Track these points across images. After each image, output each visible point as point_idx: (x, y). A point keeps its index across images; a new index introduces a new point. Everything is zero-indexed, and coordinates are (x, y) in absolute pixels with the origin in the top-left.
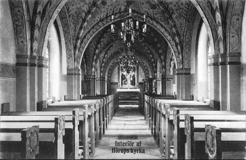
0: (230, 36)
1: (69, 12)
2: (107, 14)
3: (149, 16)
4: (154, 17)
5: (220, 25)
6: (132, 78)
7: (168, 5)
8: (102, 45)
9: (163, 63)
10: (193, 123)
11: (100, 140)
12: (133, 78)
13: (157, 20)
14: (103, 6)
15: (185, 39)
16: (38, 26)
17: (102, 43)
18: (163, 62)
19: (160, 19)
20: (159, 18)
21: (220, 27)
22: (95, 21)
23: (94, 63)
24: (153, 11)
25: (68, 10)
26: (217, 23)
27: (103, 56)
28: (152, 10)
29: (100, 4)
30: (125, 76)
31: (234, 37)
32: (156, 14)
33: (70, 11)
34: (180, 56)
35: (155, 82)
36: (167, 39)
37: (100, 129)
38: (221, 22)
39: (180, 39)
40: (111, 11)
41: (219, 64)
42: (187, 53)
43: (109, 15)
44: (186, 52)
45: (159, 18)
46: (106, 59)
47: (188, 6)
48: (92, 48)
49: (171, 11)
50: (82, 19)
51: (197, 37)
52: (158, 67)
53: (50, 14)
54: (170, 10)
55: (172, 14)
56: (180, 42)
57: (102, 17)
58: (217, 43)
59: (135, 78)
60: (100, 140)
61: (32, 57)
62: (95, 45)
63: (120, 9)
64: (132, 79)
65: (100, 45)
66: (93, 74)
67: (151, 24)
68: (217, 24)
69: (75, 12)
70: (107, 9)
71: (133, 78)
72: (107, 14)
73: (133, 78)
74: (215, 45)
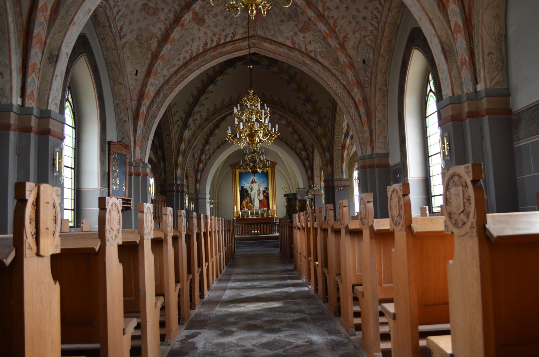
0: (483, 53)
1: (123, 37)
2: (206, 44)
3: (297, 47)
4: (306, 49)
5: (459, 31)
6: (261, 195)
7: (335, 23)
8: (197, 120)
9: (327, 154)
10: (417, 232)
11: (191, 309)
12: (265, 194)
13: (312, 55)
14: (196, 27)
15: (373, 92)
16: (41, 39)
17: (197, 116)
18: (327, 152)
19: (320, 52)
20: (318, 50)
21: (459, 35)
22: (179, 60)
23: (180, 158)
24: (304, 37)
25: (120, 33)
26: (453, 26)
27: (178, 29)
28: (301, 35)
29: (190, 21)
30: (247, 191)
31: (493, 54)
32: (310, 43)
33: (125, 35)
34: (366, 128)
35: (312, 199)
36: (336, 94)
37: (190, 282)
38: (462, 25)
39: (364, 93)
40: (215, 39)
41: (465, 115)
42: (379, 121)
43: (209, 46)
44: (377, 120)
45: (317, 50)
46: (206, 155)
47: (378, 23)
48: (176, 126)
49: (343, 34)
50: (152, 55)
51: (401, 73)
52: (315, 167)
53: (70, 13)
54: (339, 30)
55: (344, 41)
56: (365, 100)
57: (195, 50)
58: (455, 71)
59: (268, 194)
60: (192, 311)
61: (24, 110)
62: (182, 120)
63: (233, 33)
64: (262, 197)
65: (194, 121)
66: (179, 182)
67: (300, 63)
68: (453, 29)
69: (137, 37)
70: (206, 33)
71: (264, 196)
72: (206, 44)
73: (265, 194)
74: (452, 75)
